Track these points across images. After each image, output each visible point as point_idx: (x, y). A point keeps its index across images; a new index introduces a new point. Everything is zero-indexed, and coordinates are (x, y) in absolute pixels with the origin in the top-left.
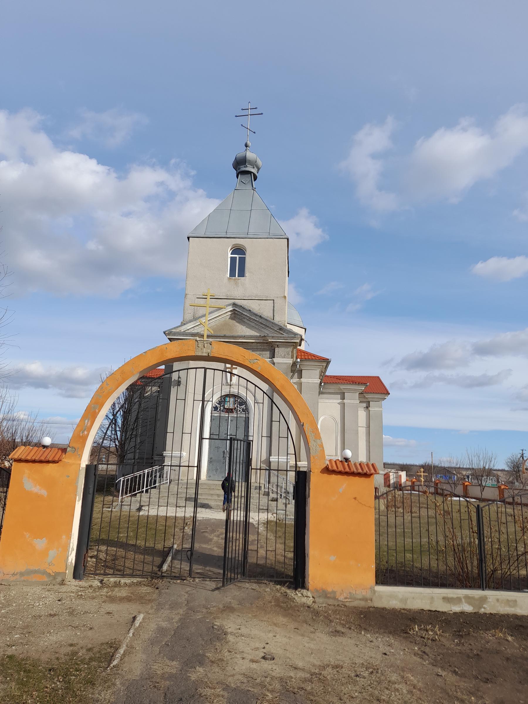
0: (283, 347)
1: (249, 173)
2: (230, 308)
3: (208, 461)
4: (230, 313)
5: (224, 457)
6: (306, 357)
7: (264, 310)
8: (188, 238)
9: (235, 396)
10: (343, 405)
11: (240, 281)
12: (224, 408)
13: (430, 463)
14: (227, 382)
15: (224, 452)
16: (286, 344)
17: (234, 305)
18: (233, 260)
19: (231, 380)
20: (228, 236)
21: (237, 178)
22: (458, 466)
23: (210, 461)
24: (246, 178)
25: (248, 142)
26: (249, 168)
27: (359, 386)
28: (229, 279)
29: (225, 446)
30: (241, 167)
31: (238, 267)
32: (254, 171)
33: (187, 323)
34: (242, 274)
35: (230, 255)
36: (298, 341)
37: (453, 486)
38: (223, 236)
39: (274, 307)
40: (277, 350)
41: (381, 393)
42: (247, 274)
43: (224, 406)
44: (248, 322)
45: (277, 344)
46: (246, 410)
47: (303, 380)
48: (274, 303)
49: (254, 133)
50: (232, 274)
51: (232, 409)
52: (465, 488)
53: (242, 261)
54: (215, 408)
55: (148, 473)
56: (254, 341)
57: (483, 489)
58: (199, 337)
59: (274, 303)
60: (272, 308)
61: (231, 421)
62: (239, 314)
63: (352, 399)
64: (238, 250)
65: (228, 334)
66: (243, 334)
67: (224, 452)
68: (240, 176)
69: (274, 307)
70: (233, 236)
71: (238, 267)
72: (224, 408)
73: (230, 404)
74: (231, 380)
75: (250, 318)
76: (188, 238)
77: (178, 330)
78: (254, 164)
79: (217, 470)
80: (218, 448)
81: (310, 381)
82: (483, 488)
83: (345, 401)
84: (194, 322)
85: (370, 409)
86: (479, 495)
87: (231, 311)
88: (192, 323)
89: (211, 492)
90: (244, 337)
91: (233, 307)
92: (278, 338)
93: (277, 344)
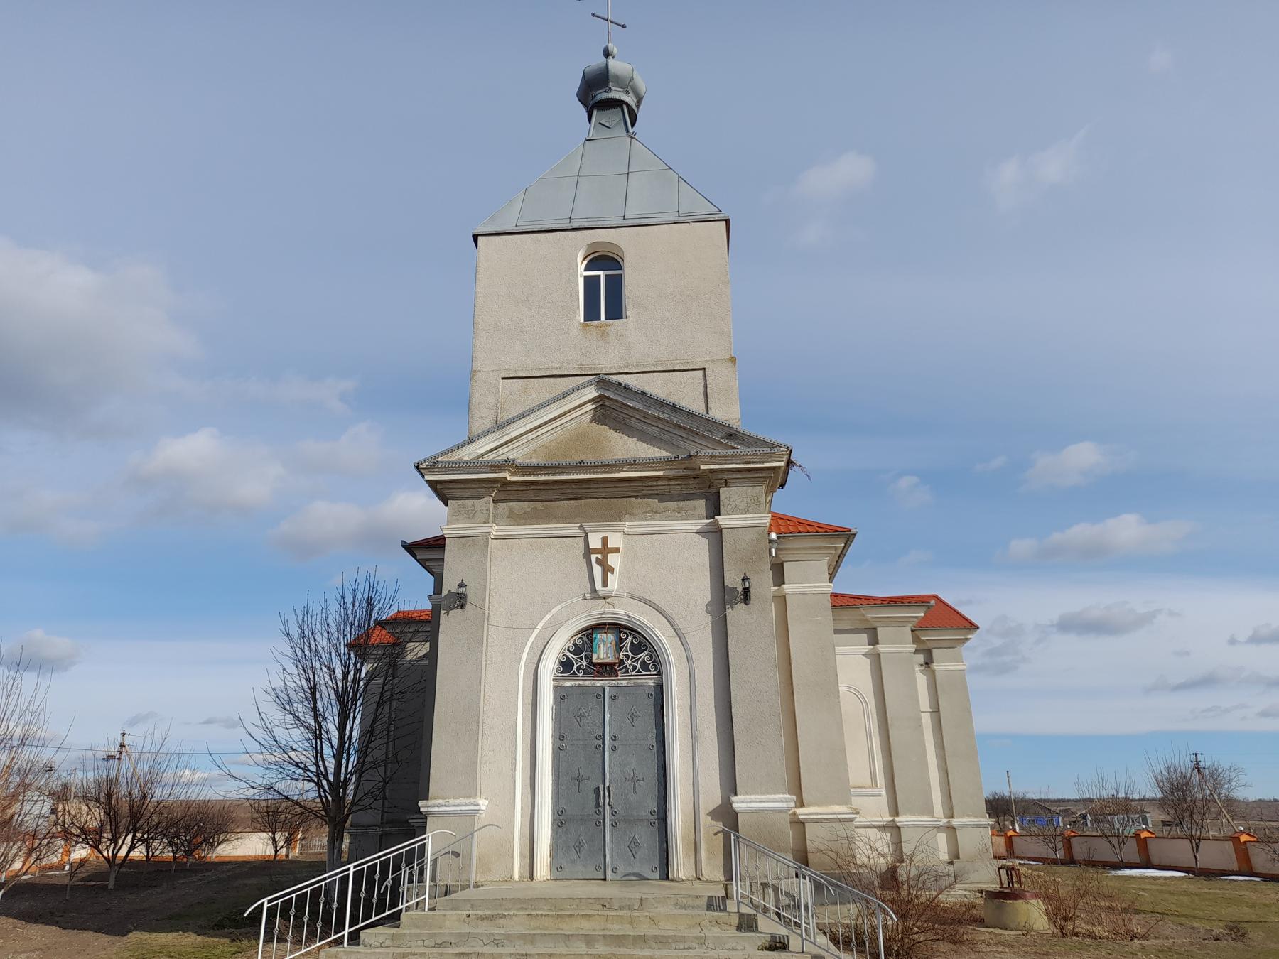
0: (742, 484)
1: (618, 104)
2: (592, 393)
3: (554, 820)
4: (591, 406)
5: (597, 805)
6: (791, 529)
7: (683, 392)
8: (475, 238)
9: (616, 627)
10: (876, 659)
11: (608, 329)
12: (590, 663)
13: (1007, 794)
14: (594, 590)
15: (597, 791)
16: (749, 476)
17: (602, 381)
18: (591, 284)
19: (605, 584)
20: (575, 225)
21: (590, 120)
22: (1122, 795)
23: (560, 820)
24: (613, 117)
25: (611, 46)
26: (617, 94)
27: (913, 609)
28: (584, 326)
29: (599, 771)
30: (600, 95)
31: (606, 294)
32: (630, 99)
33: (479, 437)
34: (616, 311)
35: (582, 272)
36: (782, 464)
37: (1115, 842)
38: (564, 226)
39: (706, 386)
40: (724, 493)
41: (958, 628)
42: (629, 310)
43: (589, 658)
44: (642, 426)
45: (725, 476)
46: (655, 664)
47: (788, 588)
48: (705, 376)
49: (624, 26)
50: (591, 313)
51: (612, 665)
52: (1143, 844)
53: (616, 286)
54: (566, 666)
55: (358, 875)
56: (661, 473)
57: (1198, 845)
58: (513, 474)
59: (705, 376)
60: (702, 389)
61: (613, 697)
62: (616, 405)
63: (898, 645)
64: (604, 260)
65: (589, 459)
66: (628, 456)
67: (597, 791)
68: (595, 112)
69: (706, 386)
70: (586, 225)
71: (606, 294)
72: (590, 663)
73: (604, 650)
74: (605, 584)
75: (646, 416)
76: (475, 238)
77: (454, 457)
78: (628, 85)
79: (580, 846)
80: (579, 779)
81: (808, 588)
82: (1196, 843)
83: (880, 648)
84: (497, 435)
85: (935, 666)
86: (1186, 858)
87: (593, 400)
88: (491, 437)
89: (567, 928)
90: (633, 465)
91: (598, 390)
92: (726, 459)
93: (725, 476)
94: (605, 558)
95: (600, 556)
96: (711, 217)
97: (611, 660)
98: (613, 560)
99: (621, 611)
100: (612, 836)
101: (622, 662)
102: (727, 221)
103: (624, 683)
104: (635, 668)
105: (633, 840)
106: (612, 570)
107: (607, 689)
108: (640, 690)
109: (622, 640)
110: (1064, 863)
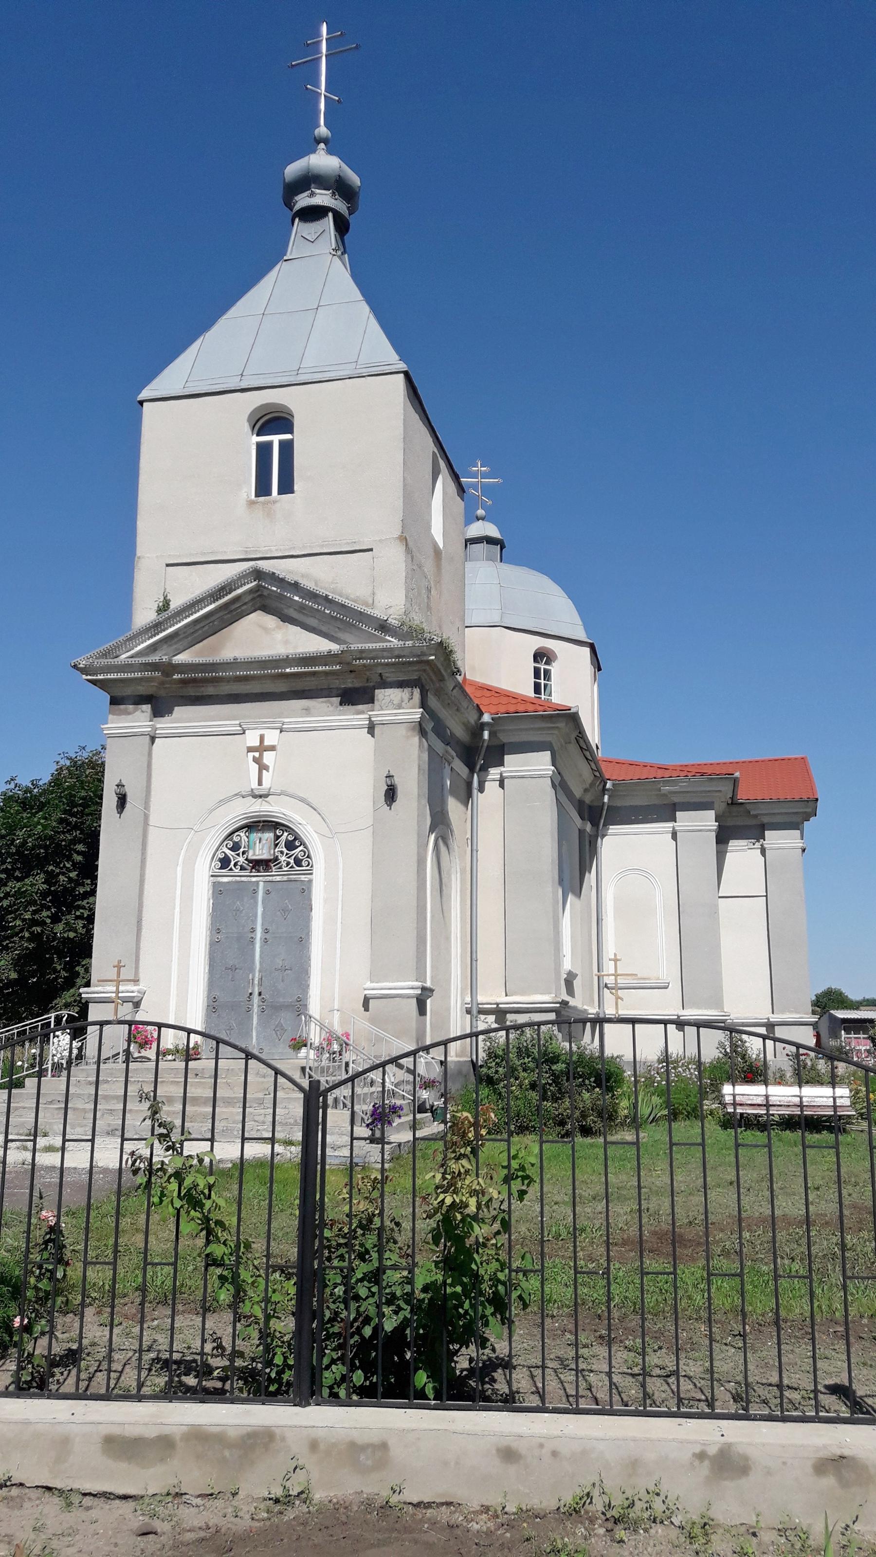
18: (264, 451)
28: (251, 503)
34: (287, 487)
50: (263, 488)
71: (275, 473)
73: (261, 846)
94: (261, 755)
95: (257, 754)
96: (388, 369)
97: (264, 856)
98: (268, 758)
99: (275, 808)
100: (259, 1020)
101: (276, 859)
102: (592, 647)
103: (278, 878)
104: (288, 864)
105: (280, 1025)
106: (267, 768)
107: (261, 884)
108: (292, 885)
109: (278, 837)
110: (770, 1149)
